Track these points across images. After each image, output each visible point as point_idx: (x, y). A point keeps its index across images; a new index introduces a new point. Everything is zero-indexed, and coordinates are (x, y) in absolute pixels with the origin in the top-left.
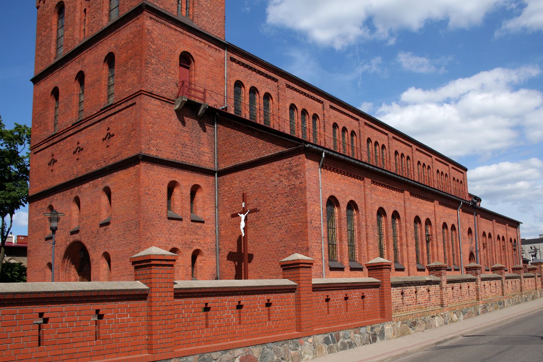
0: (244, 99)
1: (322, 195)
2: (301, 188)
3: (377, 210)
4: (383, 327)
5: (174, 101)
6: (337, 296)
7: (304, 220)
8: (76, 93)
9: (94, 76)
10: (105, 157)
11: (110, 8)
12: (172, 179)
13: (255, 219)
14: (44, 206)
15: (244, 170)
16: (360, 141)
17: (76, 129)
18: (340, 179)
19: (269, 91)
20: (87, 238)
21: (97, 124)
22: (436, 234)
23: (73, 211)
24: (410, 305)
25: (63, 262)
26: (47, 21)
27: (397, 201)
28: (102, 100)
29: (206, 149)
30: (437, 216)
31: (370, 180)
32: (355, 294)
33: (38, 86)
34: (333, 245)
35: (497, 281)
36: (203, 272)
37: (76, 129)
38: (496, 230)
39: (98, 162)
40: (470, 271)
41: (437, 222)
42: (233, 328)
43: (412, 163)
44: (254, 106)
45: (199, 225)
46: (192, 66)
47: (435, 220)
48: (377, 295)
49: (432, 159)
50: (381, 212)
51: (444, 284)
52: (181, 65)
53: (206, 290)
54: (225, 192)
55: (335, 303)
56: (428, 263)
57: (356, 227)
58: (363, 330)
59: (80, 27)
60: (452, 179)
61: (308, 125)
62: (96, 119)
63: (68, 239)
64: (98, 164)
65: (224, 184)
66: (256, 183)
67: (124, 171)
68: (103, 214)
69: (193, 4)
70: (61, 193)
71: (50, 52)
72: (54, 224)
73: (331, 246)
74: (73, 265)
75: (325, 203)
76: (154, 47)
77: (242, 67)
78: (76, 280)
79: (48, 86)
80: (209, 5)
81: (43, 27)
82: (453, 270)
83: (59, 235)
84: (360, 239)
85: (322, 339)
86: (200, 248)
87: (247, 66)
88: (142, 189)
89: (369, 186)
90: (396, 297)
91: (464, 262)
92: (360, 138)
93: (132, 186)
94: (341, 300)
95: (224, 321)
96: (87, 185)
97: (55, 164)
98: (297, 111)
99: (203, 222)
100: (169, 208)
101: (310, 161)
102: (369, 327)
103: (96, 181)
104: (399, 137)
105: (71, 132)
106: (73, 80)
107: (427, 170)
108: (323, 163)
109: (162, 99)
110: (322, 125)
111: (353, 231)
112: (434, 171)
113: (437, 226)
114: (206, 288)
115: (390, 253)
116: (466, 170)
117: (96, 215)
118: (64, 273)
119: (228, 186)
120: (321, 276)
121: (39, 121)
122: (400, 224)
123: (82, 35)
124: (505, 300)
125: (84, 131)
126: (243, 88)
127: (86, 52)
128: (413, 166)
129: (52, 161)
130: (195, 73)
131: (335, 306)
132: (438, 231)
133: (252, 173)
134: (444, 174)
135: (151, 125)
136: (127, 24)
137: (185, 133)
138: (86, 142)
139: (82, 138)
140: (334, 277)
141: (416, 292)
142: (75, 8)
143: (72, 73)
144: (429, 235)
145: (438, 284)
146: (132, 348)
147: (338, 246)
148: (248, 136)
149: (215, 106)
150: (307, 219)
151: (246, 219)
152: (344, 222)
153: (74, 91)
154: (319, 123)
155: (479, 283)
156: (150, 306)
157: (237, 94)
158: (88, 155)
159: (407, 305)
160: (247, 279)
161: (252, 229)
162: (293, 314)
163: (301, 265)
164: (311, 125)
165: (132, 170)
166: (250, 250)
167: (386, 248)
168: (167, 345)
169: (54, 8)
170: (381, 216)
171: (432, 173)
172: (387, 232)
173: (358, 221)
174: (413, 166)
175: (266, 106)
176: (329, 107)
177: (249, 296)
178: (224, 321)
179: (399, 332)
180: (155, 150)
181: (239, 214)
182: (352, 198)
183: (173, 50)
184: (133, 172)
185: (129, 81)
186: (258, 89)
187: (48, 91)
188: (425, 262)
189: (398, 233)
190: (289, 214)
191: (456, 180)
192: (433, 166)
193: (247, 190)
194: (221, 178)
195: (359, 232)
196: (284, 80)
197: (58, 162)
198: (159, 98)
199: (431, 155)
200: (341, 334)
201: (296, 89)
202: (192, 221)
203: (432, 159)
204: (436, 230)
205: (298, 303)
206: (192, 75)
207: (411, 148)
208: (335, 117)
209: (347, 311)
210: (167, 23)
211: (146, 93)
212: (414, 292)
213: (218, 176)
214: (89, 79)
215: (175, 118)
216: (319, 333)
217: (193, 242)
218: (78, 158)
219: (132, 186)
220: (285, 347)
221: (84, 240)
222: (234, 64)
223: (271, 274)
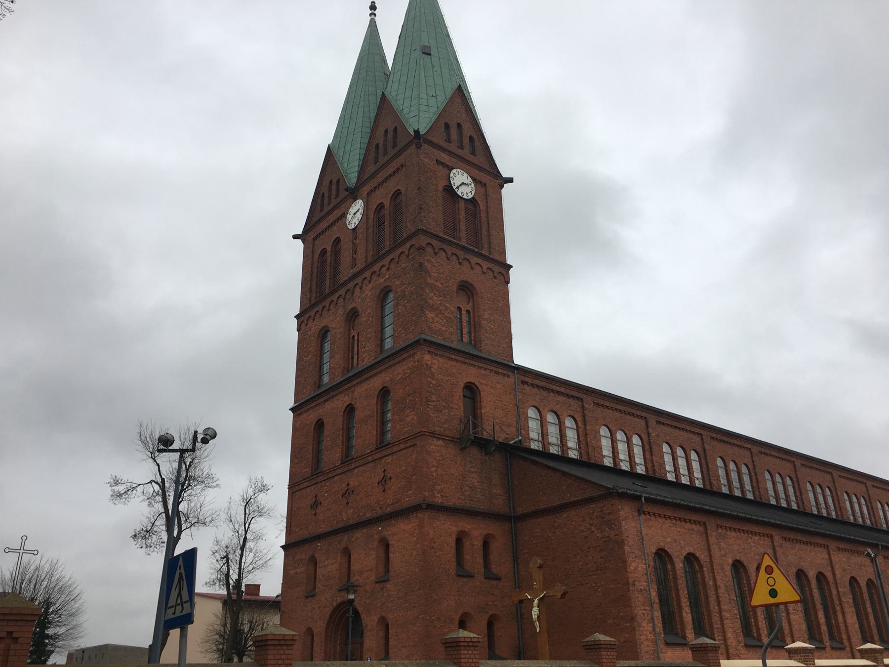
2: (618, 541)
12: (460, 529)
26: (309, 346)
41: (838, 576)
45: (494, 583)
47: (834, 575)
76: (434, 382)
81: (305, 351)
82: (828, 648)
113: (838, 582)
133: (556, 520)
135: (433, 469)
137: (473, 474)
176: (654, 423)
180: (439, 495)
183: (455, 383)
187: (311, 422)
188: (824, 637)
190: (606, 573)
217: (488, 605)
219: (415, 539)
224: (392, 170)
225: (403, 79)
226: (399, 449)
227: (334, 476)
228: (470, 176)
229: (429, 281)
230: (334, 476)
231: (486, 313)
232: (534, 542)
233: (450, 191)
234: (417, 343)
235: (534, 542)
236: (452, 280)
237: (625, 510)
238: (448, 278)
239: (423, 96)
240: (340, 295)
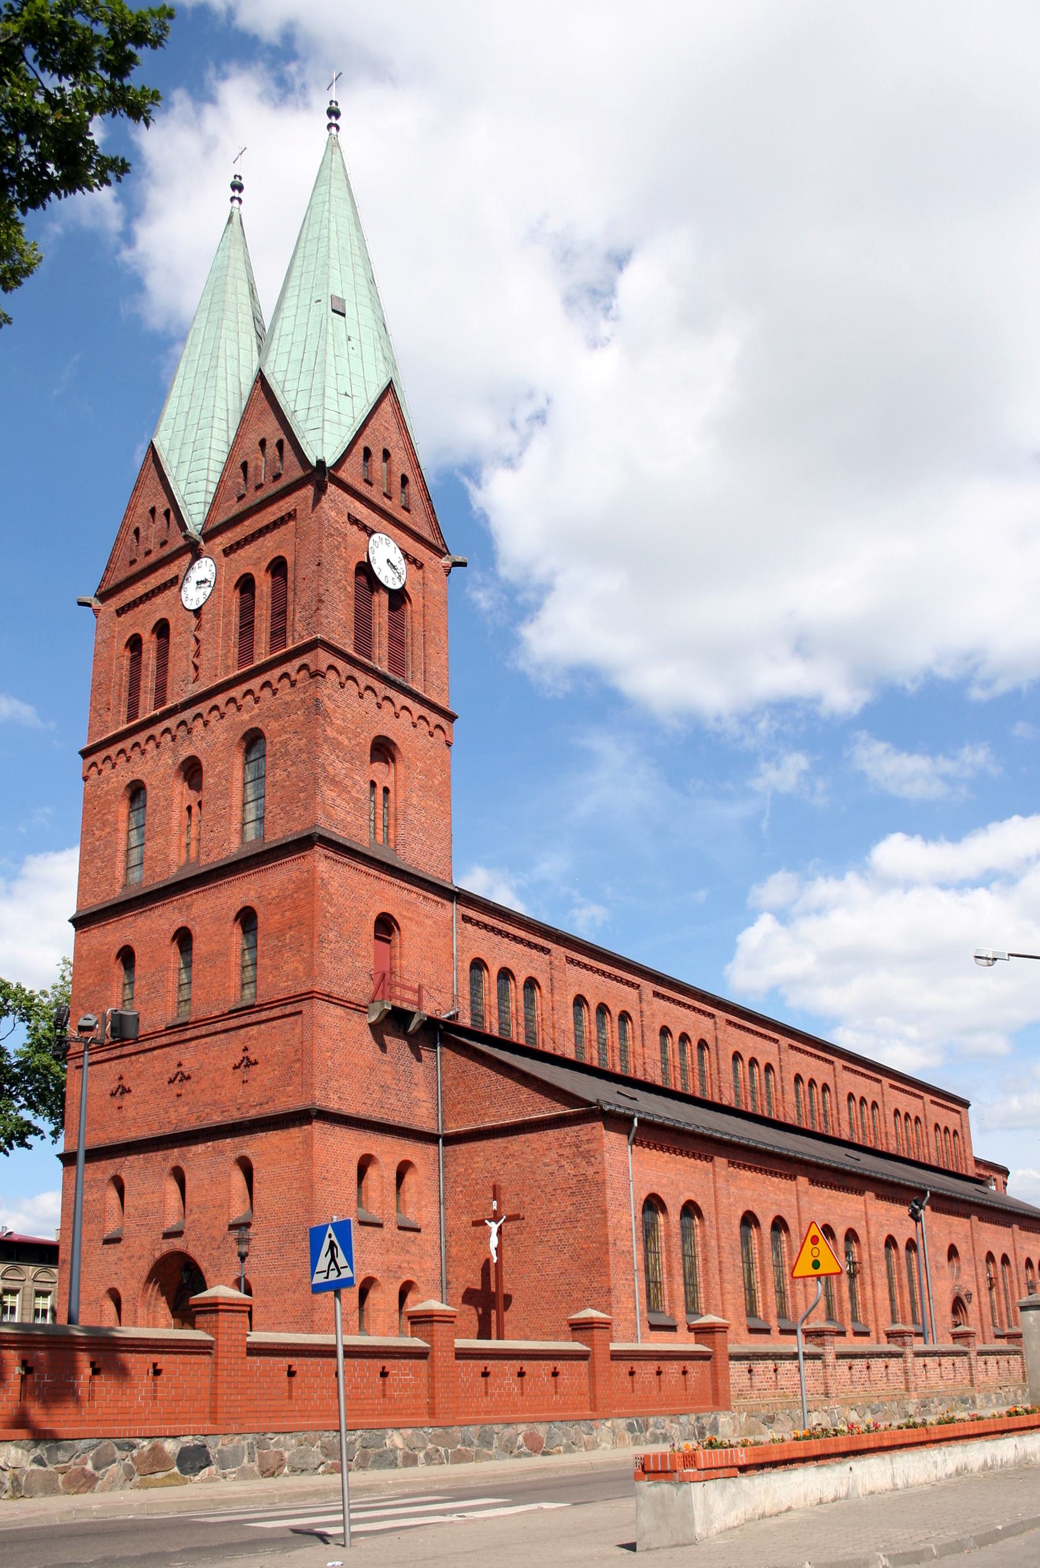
0: (487, 993)
1: (635, 1192)
3: (740, 1217)
4: (715, 1419)
5: (366, 1007)
6: (646, 1370)
7: (603, 1239)
8: (172, 965)
9: (214, 944)
10: (239, 1101)
11: (243, 818)
12: (365, 1151)
13: (515, 1231)
14: (100, 1176)
15: (494, 1138)
16: (718, 1059)
17: (175, 1038)
18: (667, 1162)
19: (534, 974)
20: (200, 1248)
21: (222, 1036)
22: (871, 1261)
24: (765, 1389)
25: (145, 1289)
27: (782, 1197)
28: (232, 991)
29: (422, 1094)
30: (872, 1223)
31: (725, 1161)
32: (672, 1368)
33: (85, 935)
34: (656, 1282)
35: (957, 1360)
37: (175, 1038)
38: (1022, 1248)
40: (894, 1339)
41: (873, 1235)
42: (514, 1399)
43: (833, 1098)
44: (506, 1004)
46: (396, 938)
47: (868, 1232)
48: (708, 1372)
49: (882, 1086)
50: (749, 1220)
51: (830, 1359)
52: (376, 937)
53: (486, 1352)
54: (458, 1175)
55: (643, 1378)
56: (1020, 1298)
57: (700, 1249)
58: (683, 1419)
59: (180, 840)
60: (931, 1129)
61: (609, 1036)
62: (219, 1026)
63: (159, 1246)
64: (224, 1112)
65: (455, 1160)
67: (279, 1132)
69: (396, 820)
70: (142, 1156)
71: (114, 873)
72: (244, 1249)
73: (652, 1285)
74: (163, 1295)
75: (640, 1208)
76: (332, 910)
77: (484, 931)
78: (168, 1326)
79: (109, 939)
80: (423, 819)
81: (98, 820)
82: (849, 1334)
83: (137, 1236)
84: (706, 1272)
85: (624, 1424)
86: (414, 1279)
87: (492, 929)
88: (317, 1170)
89: (724, 1173)
90: (740, 1376)
91: (939, 1318)
92: (717, 1054)
93: (297, 1163)
94: (651, 1373)
95: (505, 1389)
96: (200, 1148)
97: (127, 1096)
98: (588, 1009)
99: (418, 1230)
100: (360, 1203)
101: (611, 1134)
102: (693, 1417)
103: (220, 1143)
104: (803, 1043)
105: (164, 1040)
106: (168, 941)
107: (870, 1112)
108: (636, 1135)
109: (346, 1004)
110: (638, 1033)
111: (695, 1257)
112: (887, 1112)
113: (872, 1243)
114: (486, 1349)
115: (769, 1300)
116: (966, 1104)
117: (221, 1206)
118: (146, 1312)
119: (463, 1164)
120: (634, 1339)
121: (87, 1004)
122: (789, 1241)
123: (184, 855)
124: (977, 1395)
125: (193, 1043)
126: (485, 971)
127: (196, 893)
128: (837, 1104)
129: (118, 1089)
130: (401, 953)
131: (643, 1382)
132: (873, 1253)
133: (509, 1145)
134: (913, 1117)
135: (329, 1054)
136: (282, 861)
137: (386, 1066)
138: (197, 1066)
139: (189, 1056)
140: (657, 1341)
141: (775, 1370)
142: (170, 801)
143: (166, 927)
144: (855, 1263)
145: (820, 1359)
146: (414, 1411)
147: (666, 1286)
148: (500, 1077)
149: (438, 1012)
150: (607, 1238)
151: (500, 1232)
152: (677, 1241)
153: (169, 961)
154: (633, 1029)
155: (909, 1360)
156: (433, 1367)
157: (475, 983)
158: (203, 1091)
159: (760, 1390)
160: (503, 1339)
161: (509, 1248)
162: (586, 1388)
163: (595, 1325)
164: (616, 1034)
165: (296, 1133)
166: (507, 1288)
167: (760, 1289)
168: (449, 1410)
169: (123, 789)
170: (750, 1227)
171: (882, 1118)
172: (762, 1259)
173: (704, 1237)
174: (837, 1104)
175: (529, 1002)
177: (532, 1362)
178: (505, 1389)
179: (744, 1428)
180: (336, 1098)
182: (691, 1196)
183: (364, 913)
185: (288, 968)
186: (513, 971)
188: (846, 1317)
189: (787, 1260)
191: (942, 1128)
192: (883, 1102)
194: (449, 1148)
195: (705, 1260)
196: (563, 949)
197: (132, 1093)
198: (342, 1003)
199: (879, 1077)
200: (651, 1420)
201: (585, 964)
202: (400, 1228)
203: (882, 1086)
204: (870, 1252)
205: (592, 1374)
207: (831, 1066)
208: (665, 1014)
209: (660, 1390)
210: (354, 864)
211: (320, 996)
212: (772, 1370)
213: (444, 1145)
214: (202, 946)
215: (368, 1038)
216: (620, 1416)
218: (179, 1092)
219: (297, 1163)
220: (575, 1429)
221: (194, 1252)
222: (469, 926)
223: (545, 1334)
224: (272, 519)
225: (297, 355)
228: (400, 549)
229: (330, 732)
231: (413, 794)
233: (365, 570)
234: (304, 843)
236: (365, 734)
237: (613, 1141)
238: (358, 730)
239: (330, 392)
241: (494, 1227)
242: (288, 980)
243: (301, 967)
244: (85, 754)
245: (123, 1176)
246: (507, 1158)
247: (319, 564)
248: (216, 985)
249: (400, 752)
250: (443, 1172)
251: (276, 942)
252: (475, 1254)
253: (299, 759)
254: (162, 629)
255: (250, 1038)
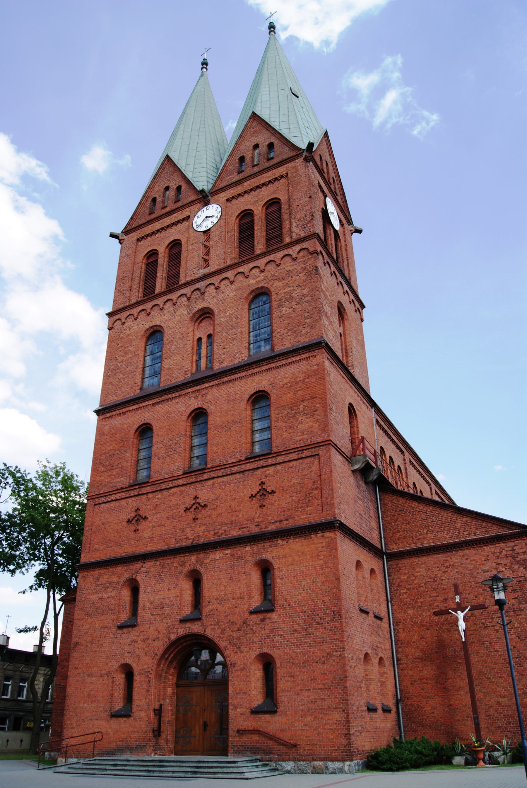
10: (256, 520)
23: (184, 590)
36: (385, 690)
39: (242, 525)
54: (401, 582)
66: (457, 572)
68: (254, 597)
106: (184, 418)
119: (405, 574)
121: (107, 463)
133: (449, 559)
151: (465, 619)
181: (450, 611)
184: (322, 543)
190: (521, 615)
193: (442, 580)
197: (149, 520)
206: (354, 432)
219: (321, 562)
226: (288, 459)
227: (171, 488)
230: (171, 488)
232: (415, 582)
235: (415, 582)
240: (157, 305)
241: (461, 615)
242: (303, 434)
243: (316, 425)
244: (109, 315)
245: (139, 578)
246: (447, 567)
247: (310, 197)
248: (232, 442)
249: (347, 315)
250: (389, 580)
251: (290, 411)
252: (423, 638)
253: (303, 301)
254: (175, 245)
255: (266, 476)
